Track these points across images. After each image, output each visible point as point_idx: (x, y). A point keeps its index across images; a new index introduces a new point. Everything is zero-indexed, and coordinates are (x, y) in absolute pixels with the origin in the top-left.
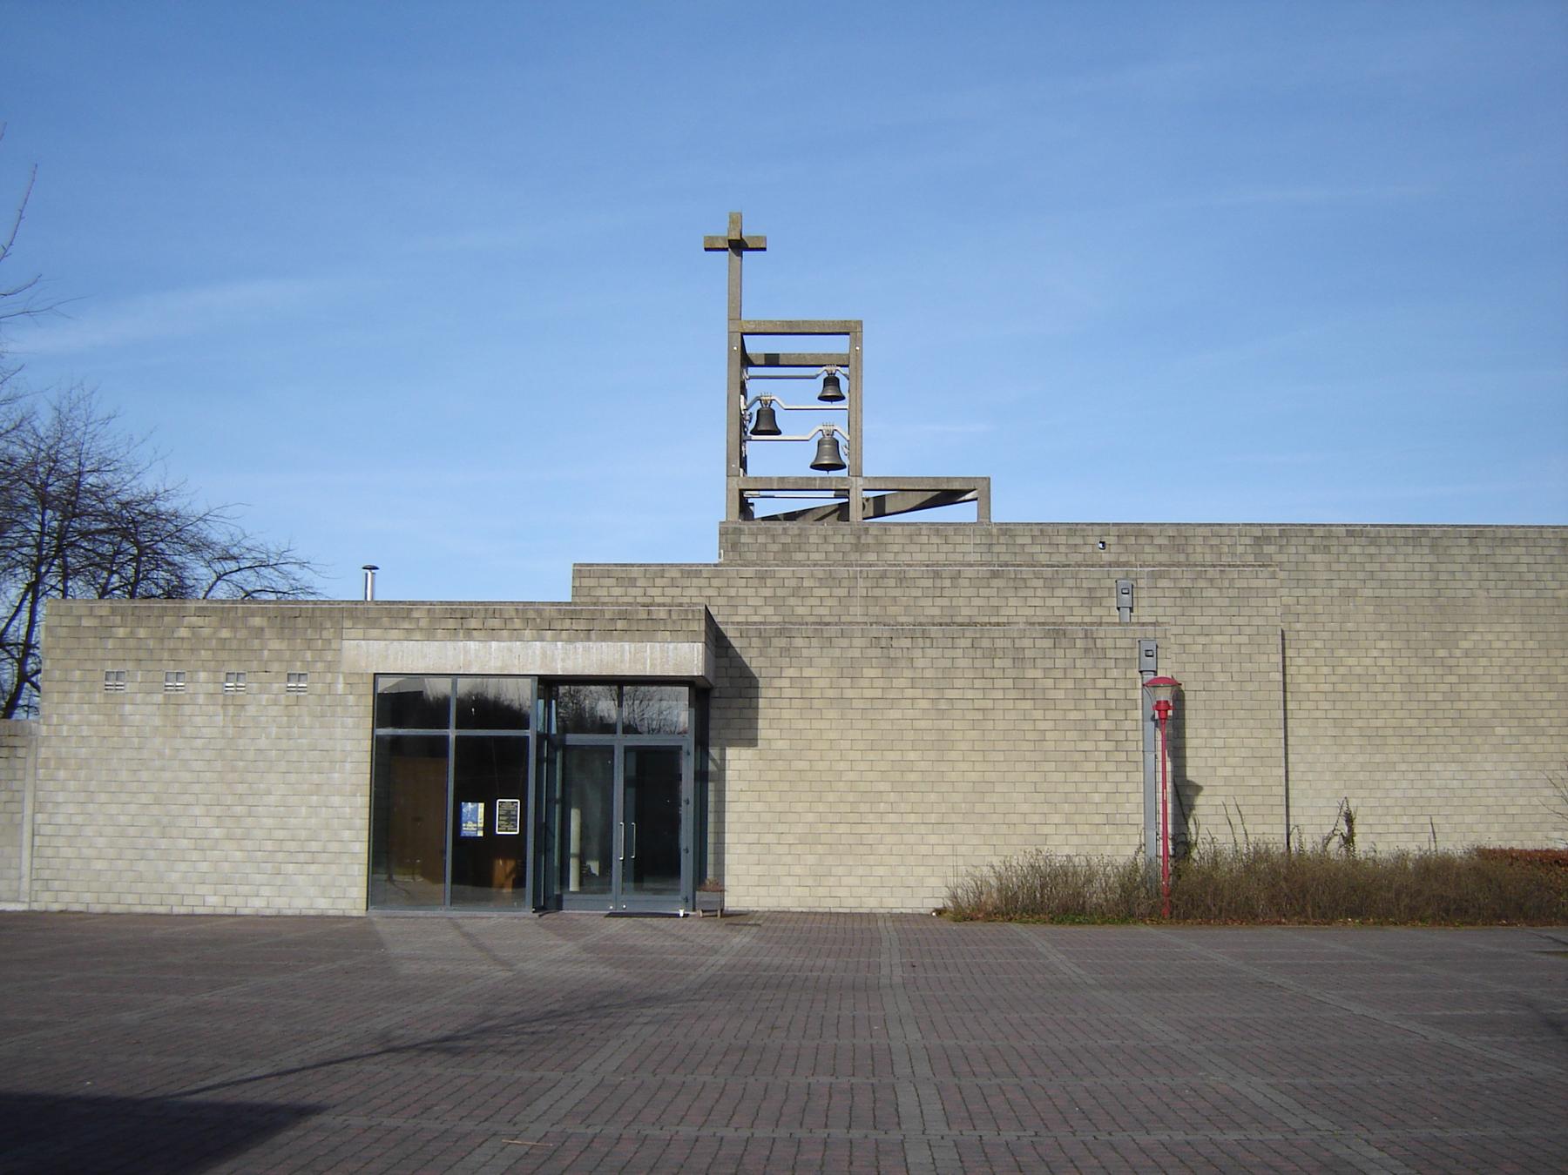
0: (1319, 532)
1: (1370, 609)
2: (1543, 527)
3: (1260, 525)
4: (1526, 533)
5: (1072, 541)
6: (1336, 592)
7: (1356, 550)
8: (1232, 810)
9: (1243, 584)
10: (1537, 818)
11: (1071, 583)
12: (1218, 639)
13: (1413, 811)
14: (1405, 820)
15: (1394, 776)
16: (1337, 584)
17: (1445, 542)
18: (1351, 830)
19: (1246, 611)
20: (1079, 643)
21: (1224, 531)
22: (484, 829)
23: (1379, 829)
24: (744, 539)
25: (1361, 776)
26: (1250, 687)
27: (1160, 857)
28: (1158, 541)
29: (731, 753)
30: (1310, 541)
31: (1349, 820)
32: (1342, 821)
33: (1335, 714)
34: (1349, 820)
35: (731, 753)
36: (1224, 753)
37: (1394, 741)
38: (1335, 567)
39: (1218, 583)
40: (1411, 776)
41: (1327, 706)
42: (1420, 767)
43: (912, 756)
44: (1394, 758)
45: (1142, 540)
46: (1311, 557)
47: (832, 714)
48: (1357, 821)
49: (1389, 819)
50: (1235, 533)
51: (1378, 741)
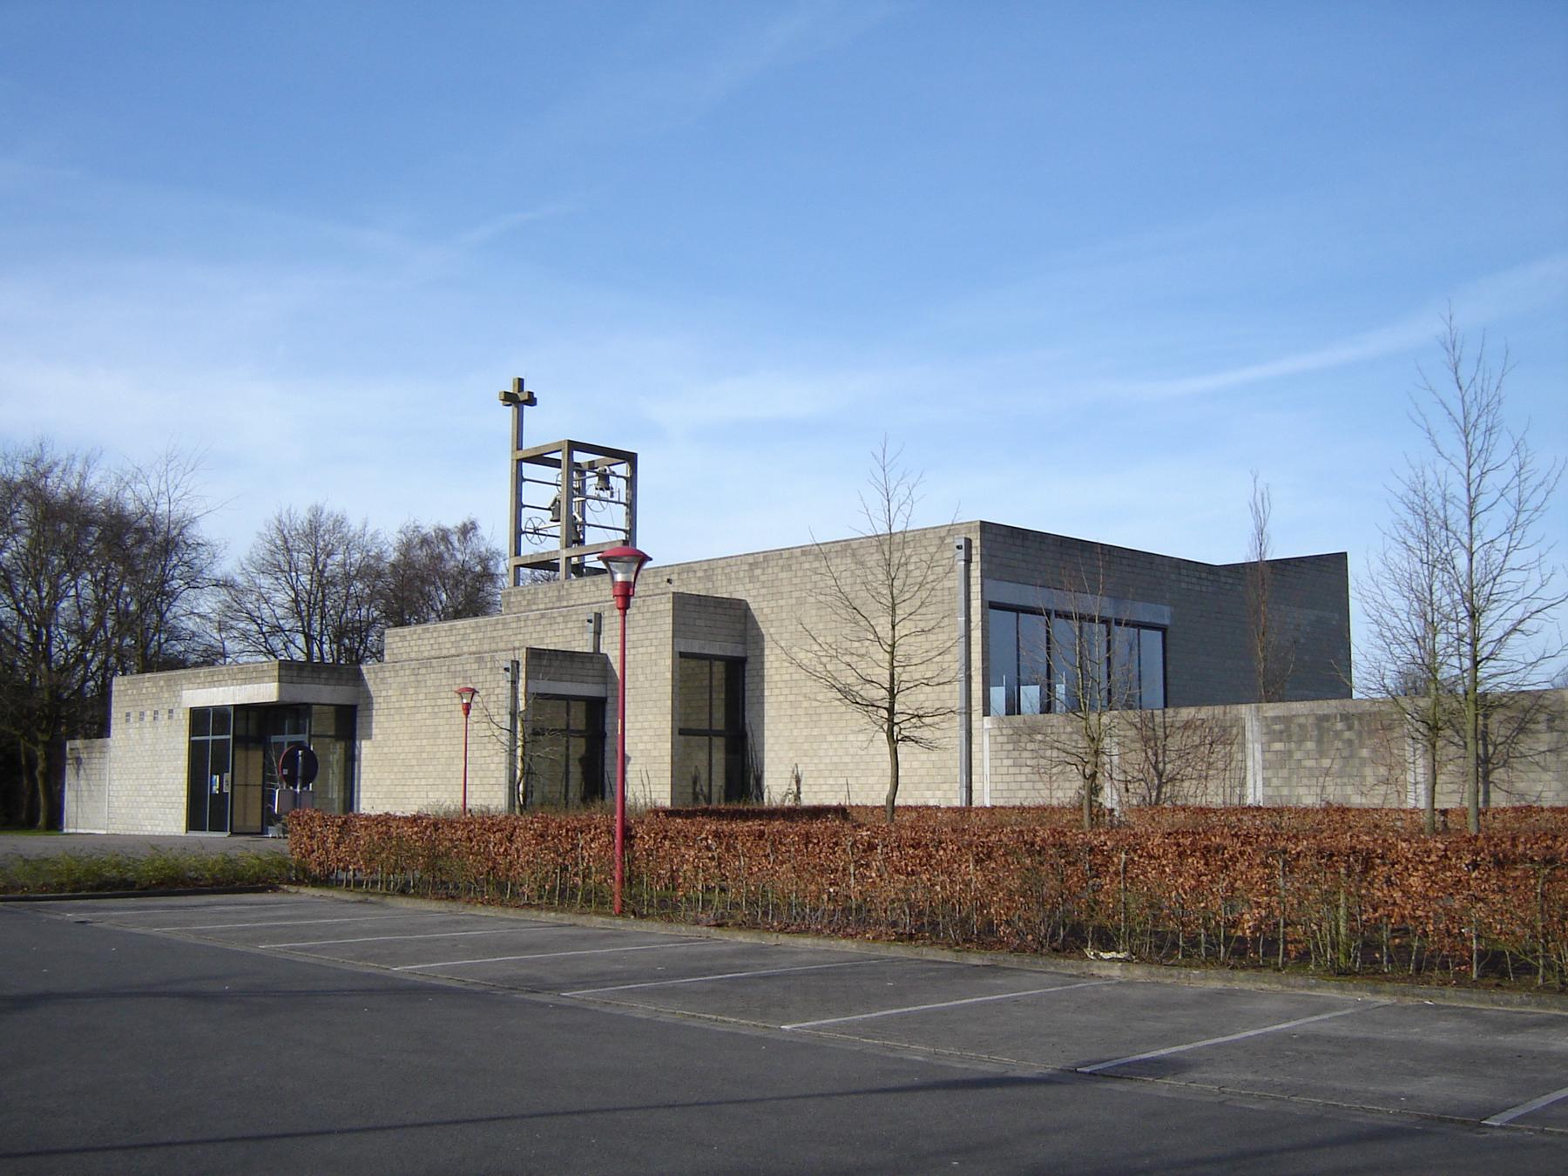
0: (786, 554)
1: (814, 612)
2: (926, 529)
3: (753, 554)
4: (915, 536)
5: (656, 580)
6: (794, 601)
7: (807, 566)
8: (644, 774)
9: (652, 609)
10: (916, 779)
11: (574, 617)
12: (640, 650)
13: (836, 773)
14: (831, 781)
15: (825, 746)
16: (795, 594)
17: (862, 551)
18: (798, 789)
19: (655, 629)
20: (489, 665)
21: (733, 561)
22: (219, 789)
23: (815, 789)
24: (513, 599)
25: (806, 746)
26: (655, 684)
27: (934, 794)
28: (699, 574)
29: (363, 743)
30: (781, 562)
31: (798, 781)
32: (794, 783)
33: (791, 698)
34: (798, 781)
35: (363, 743)
36: (641, 733)
37: (825, 717)
38: (795, 581)
39: (642, 610)
40: (836, 745)
41: (786, 691)
42: (841, 738)
43: (424, 742)
44: (825, 731)
45: (691, 575)
46: (781, 575)
47: (397, 717)
48: (802, 782)
49: (821, 781)
50: (739, 562)
51: (815, 718)
